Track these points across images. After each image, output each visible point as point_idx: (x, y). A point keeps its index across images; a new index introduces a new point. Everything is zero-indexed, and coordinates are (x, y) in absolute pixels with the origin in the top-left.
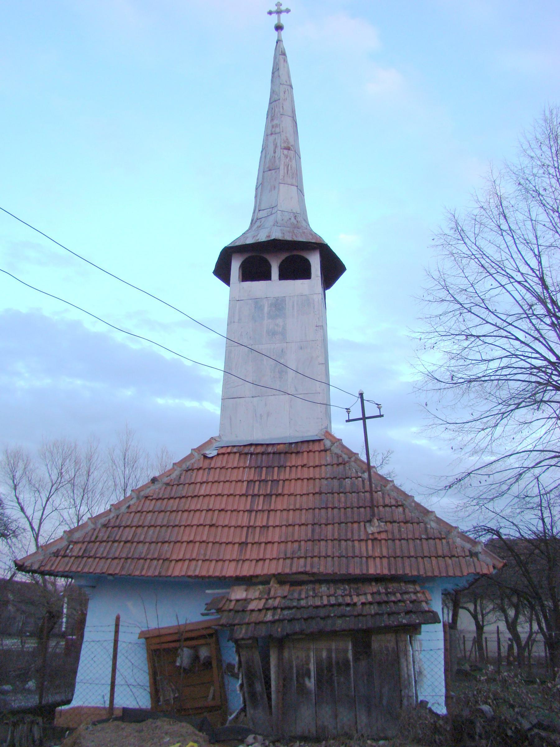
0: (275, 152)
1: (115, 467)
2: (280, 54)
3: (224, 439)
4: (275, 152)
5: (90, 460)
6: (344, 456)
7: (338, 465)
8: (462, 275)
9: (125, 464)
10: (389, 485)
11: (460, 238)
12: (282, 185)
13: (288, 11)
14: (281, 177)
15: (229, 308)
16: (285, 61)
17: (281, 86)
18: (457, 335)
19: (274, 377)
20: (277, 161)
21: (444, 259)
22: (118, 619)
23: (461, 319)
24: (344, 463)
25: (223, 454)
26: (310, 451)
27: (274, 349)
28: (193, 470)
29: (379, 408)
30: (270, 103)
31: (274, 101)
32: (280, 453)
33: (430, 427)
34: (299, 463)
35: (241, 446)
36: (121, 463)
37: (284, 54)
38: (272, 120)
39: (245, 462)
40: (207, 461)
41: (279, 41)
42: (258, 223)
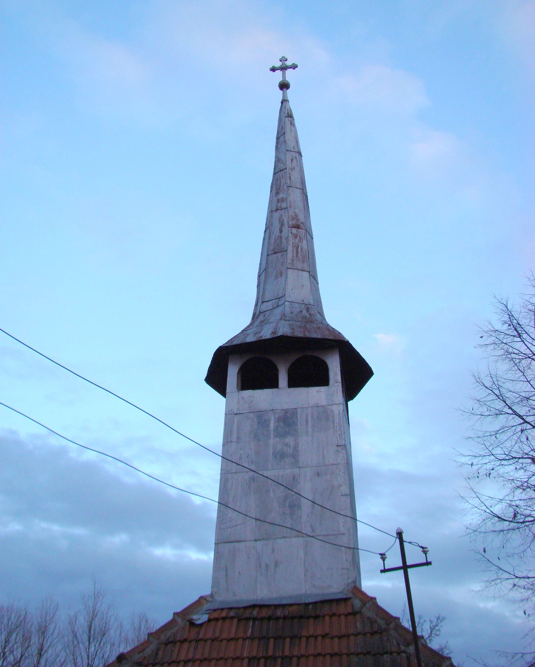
0: (281, 231)
1: (76, 643)
2: (286, 116)
3: (218, 598)
4: (281, 231)
5: (43, 633)
6: (380, 621)
7: (372, 634)
8: (523, 378)
9: (90, 638)
10: (444, 664)
11: (516, 334)
12: (290, 272)
13: (294, 67)
14: (289, 261)
15: (225, 424)
16: (292, 124)
17: (288, 153)
18: (519, 458)
19: (284, 513)
20: (284, 241)
21: (496, 361)
23: (524, 439)
24: (380, 632)
25: (217, 619)
26: (334, 615)
27: (283, 476)
28: (174, 642)
29: (425, 552)
30: (275, 174)
31: (279, 171)
32: (293, 618)
33: (493, 583)
34: (319, 631)
35: (240, 608)
36: (85, 637)
37: (290, 116)
38: (277, 193)
39: (246, 631)
40: (194, 630)
41: (284, 101)
42: (261, 318)
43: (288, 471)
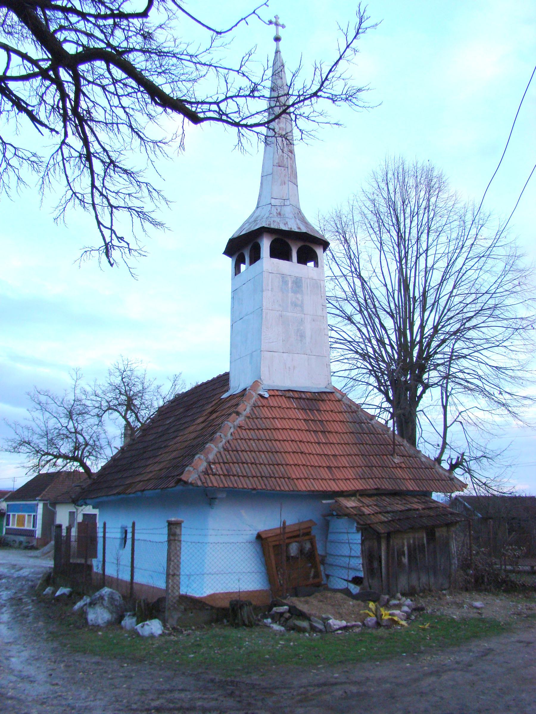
22: (105, 524)
24: (355, 412)
41: (277, 52)
43: (299, 315)
